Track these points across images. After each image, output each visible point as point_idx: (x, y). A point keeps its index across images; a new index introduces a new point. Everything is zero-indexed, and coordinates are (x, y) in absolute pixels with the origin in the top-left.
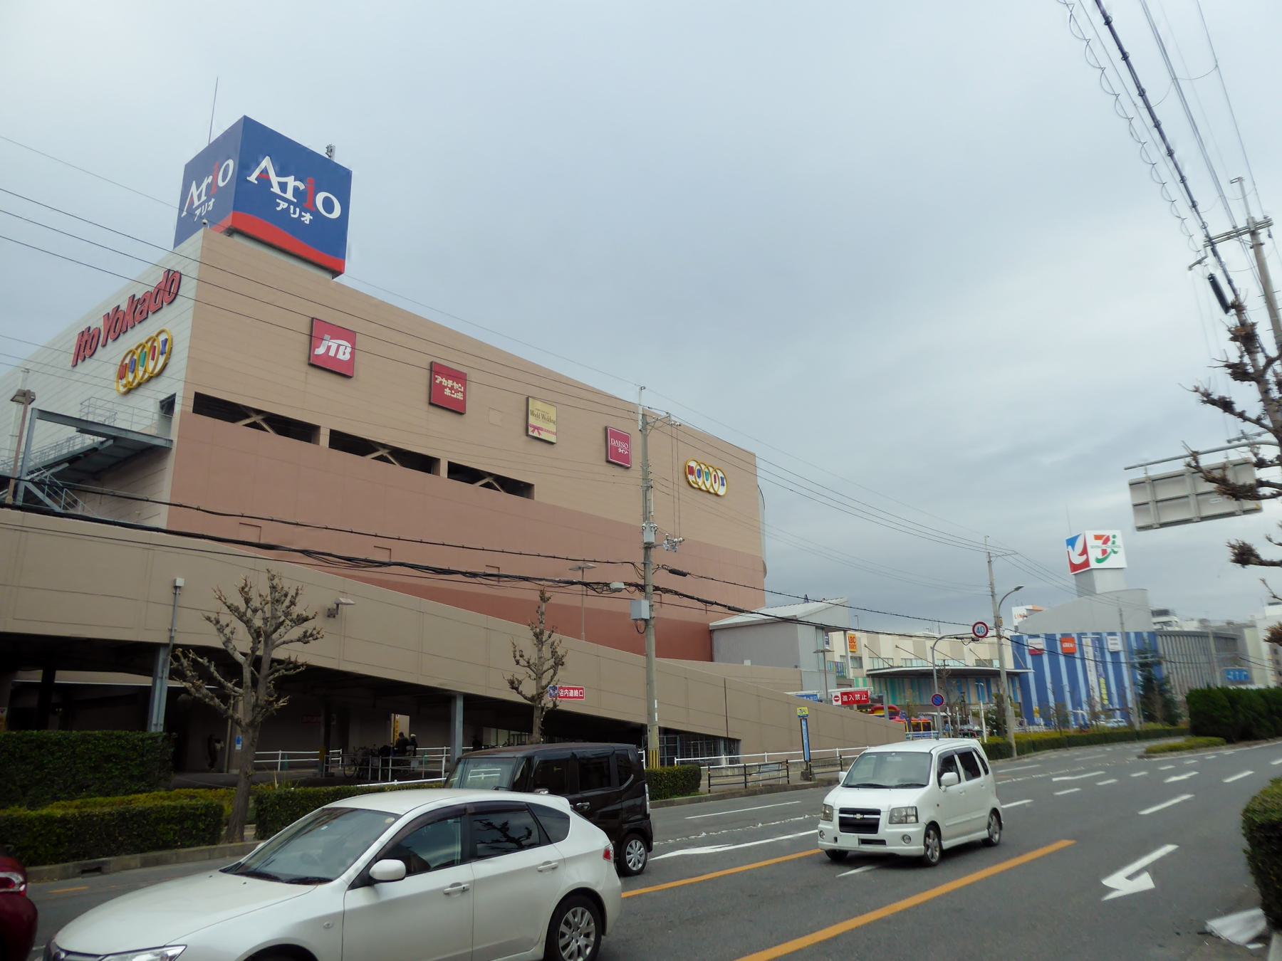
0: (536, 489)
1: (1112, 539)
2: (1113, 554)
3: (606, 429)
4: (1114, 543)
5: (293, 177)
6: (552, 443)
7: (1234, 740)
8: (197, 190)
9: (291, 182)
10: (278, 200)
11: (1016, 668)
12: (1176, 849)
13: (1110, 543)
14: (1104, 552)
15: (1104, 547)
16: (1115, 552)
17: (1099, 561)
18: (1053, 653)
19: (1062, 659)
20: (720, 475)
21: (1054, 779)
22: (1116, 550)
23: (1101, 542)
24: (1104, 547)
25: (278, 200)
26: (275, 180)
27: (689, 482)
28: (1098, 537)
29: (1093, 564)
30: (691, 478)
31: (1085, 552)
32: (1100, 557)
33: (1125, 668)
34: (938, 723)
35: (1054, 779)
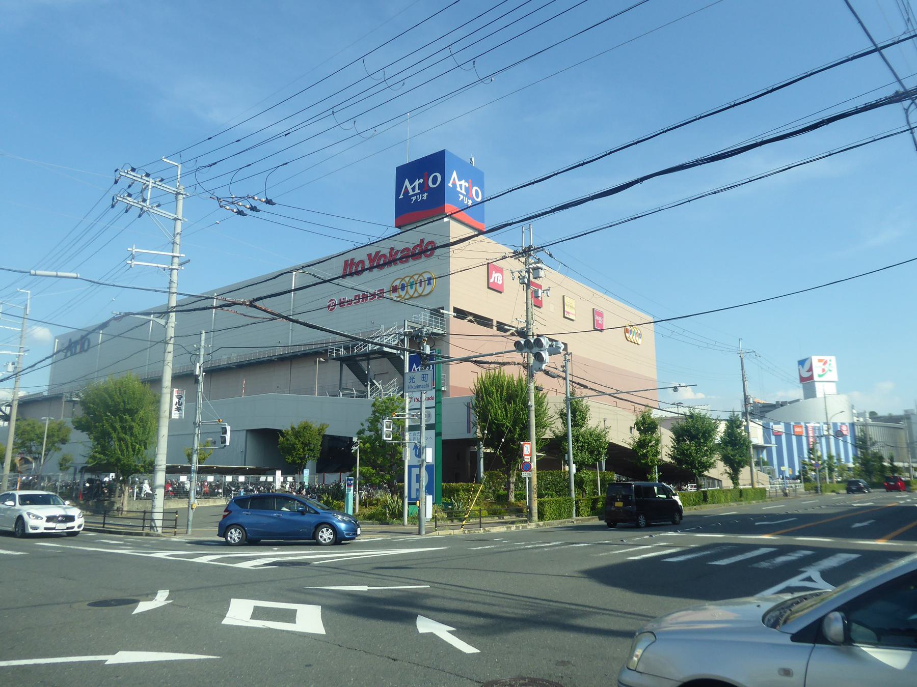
0: (777, 401)
1: (829, 362)
2: (829, 372)
3: (593, 309)
4: (830, 365)
5: (464, 181)
6: (573, 320)
7: (902, 490)
8: (406, 186)
9: (463, 183)
10: (460, 195)
11: (765, 443)
12: (861, 556)
13: (827, 365)
14: (824, 370)
15: (824, 367)
16: (830, 371)
17: (820, 376)
18: (788, 435)
19: (794, 438)
20: (639, 332)
21: (757, 524)
22: (831, 369)
23: (822, 363)
24: (824, 367)
25: (460, 195)
26: (458, 183)
27: (626, 337)
28: (820, 361)
29: (816, 378)
30: (627, 335)
31: (811, 369)
32: (821, 373)
33: (850, 446)
34: (414, 509)
35: (757, 524)
